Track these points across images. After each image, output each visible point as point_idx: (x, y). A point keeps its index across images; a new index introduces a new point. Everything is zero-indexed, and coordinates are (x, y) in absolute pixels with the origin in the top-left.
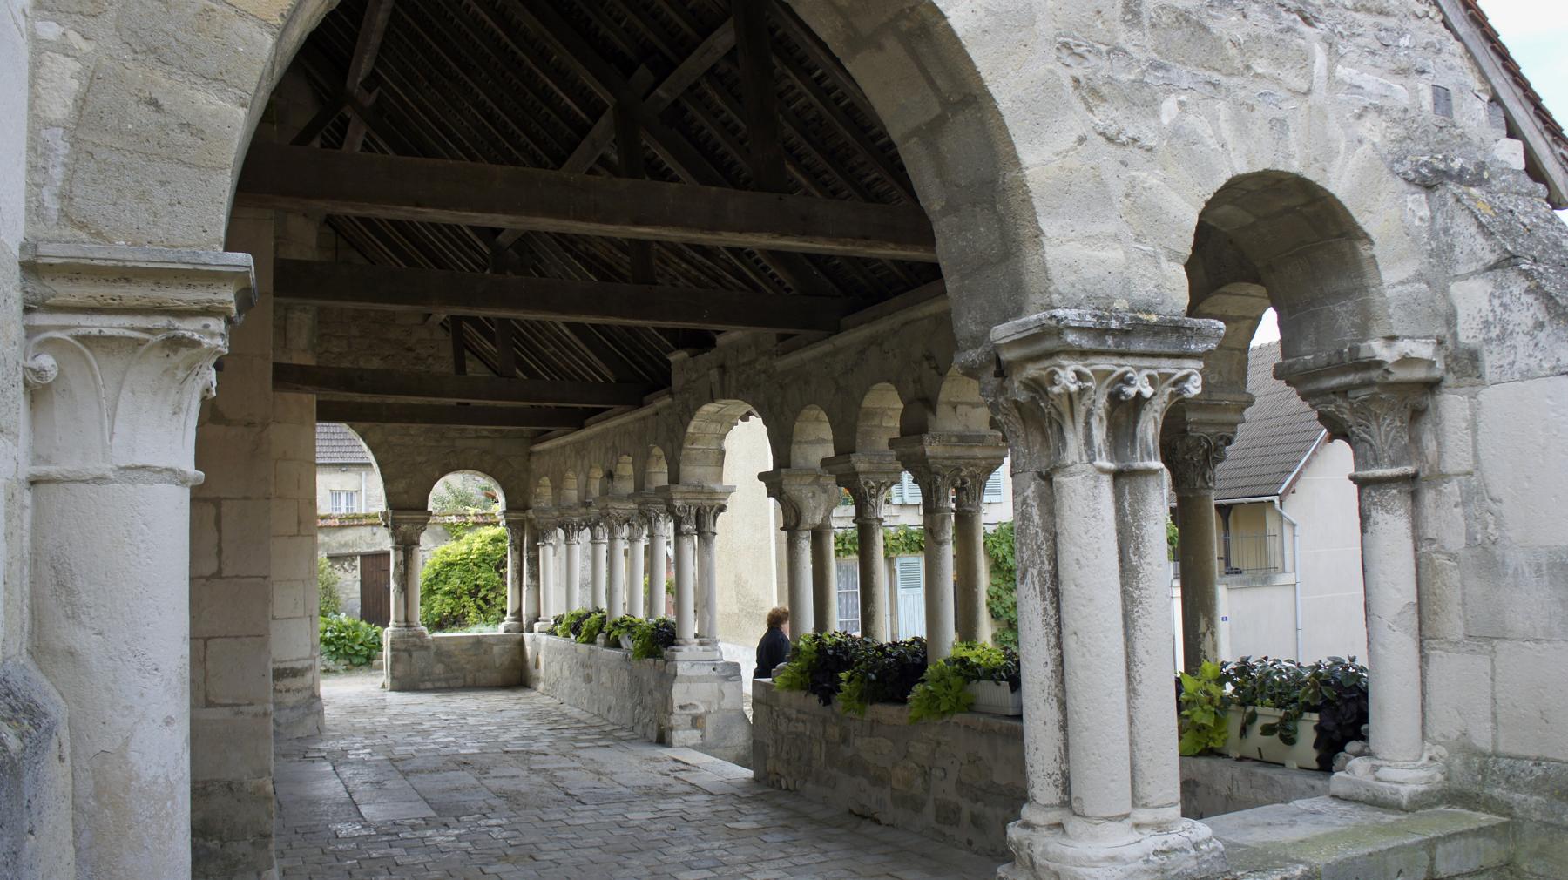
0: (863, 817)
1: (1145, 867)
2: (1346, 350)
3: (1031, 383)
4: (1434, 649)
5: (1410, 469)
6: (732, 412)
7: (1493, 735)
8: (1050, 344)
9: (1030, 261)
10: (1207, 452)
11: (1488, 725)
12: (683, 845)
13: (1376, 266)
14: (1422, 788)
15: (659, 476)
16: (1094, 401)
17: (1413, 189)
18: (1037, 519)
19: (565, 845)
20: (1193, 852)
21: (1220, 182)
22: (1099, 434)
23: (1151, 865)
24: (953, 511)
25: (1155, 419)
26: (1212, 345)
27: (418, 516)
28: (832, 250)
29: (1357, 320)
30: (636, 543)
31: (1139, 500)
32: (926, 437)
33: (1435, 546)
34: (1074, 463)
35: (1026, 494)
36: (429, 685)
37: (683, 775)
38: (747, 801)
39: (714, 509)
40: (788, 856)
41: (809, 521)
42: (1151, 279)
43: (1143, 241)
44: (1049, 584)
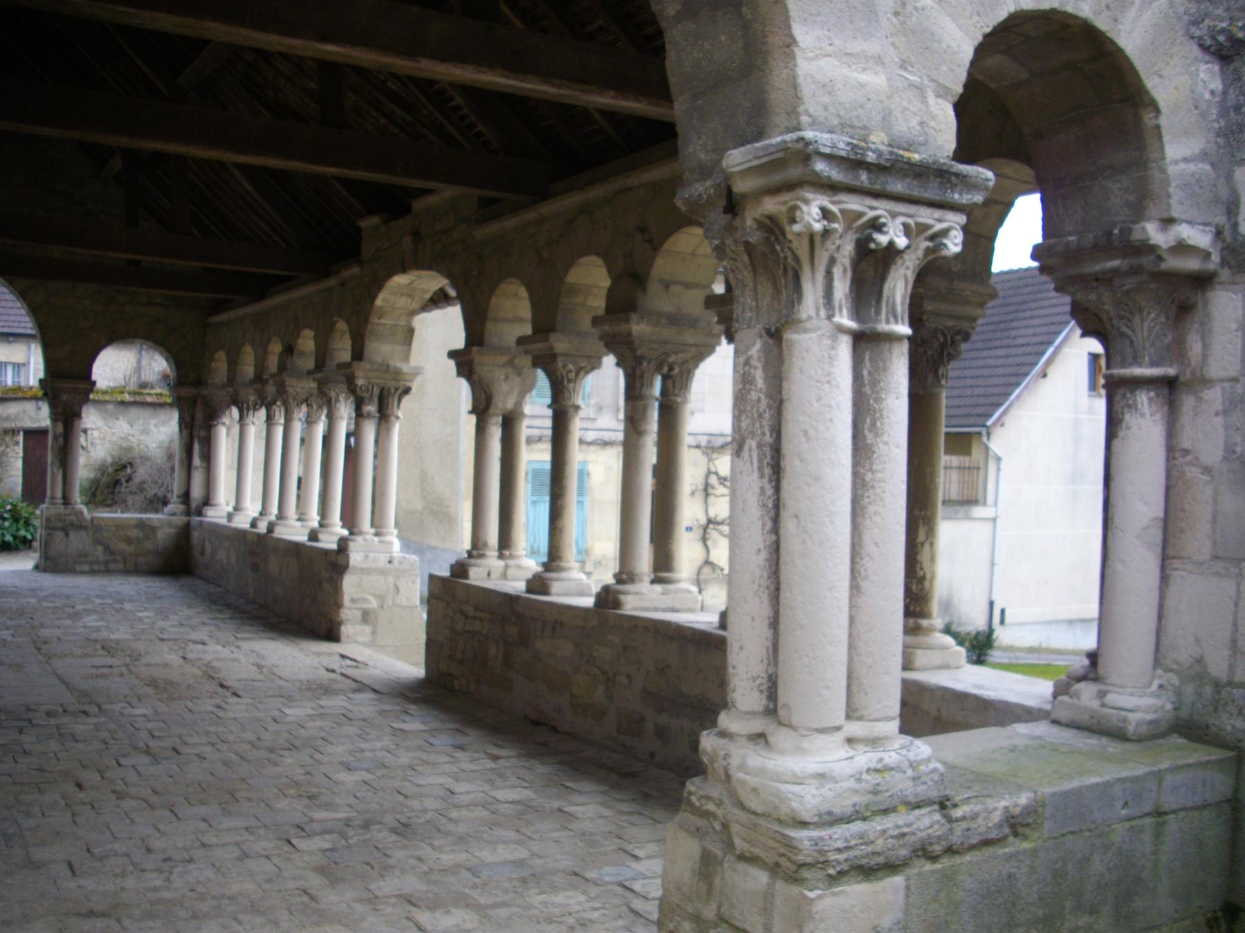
0: (537, 723)
1: (857, 786)
2: (1116, 231)
3: (768, 222)
4: (1177, 569)
5: (1171, 371)
6: (424, 286)
7: (1230, 665)
8: (794, 172)
9: (778, 77)
10: (943, 346)
11: (1226, 653)
12: (343, 744)
13: (1160, 137)
14: (1150, 717)
15: (343, 352)
16: (839, 248)
17: (1207, 58)
18: (760, 383)
19: (214, 739)
20: (910, 773)
21: (1001, 15)
22: (841, 288)
23: (863, 785)
24: (657, 399)
25: (906, 277)
26: (979, 198)
27: (81, 386)
28: (545, 93)
29: (1132, 198)
30: (314, 425)
31: (880, 368)
32: (634, 317)
33: (1189, 458)
34: (810, 318)
35: (749, 353)
36: (86, 568)
37: (350, 672)
38: (416, 701)
39: (400, 391)
40: (455, 761)
41: (500, 405)
42: (915, 114)
43: (910, 69)
44: (769, 457)
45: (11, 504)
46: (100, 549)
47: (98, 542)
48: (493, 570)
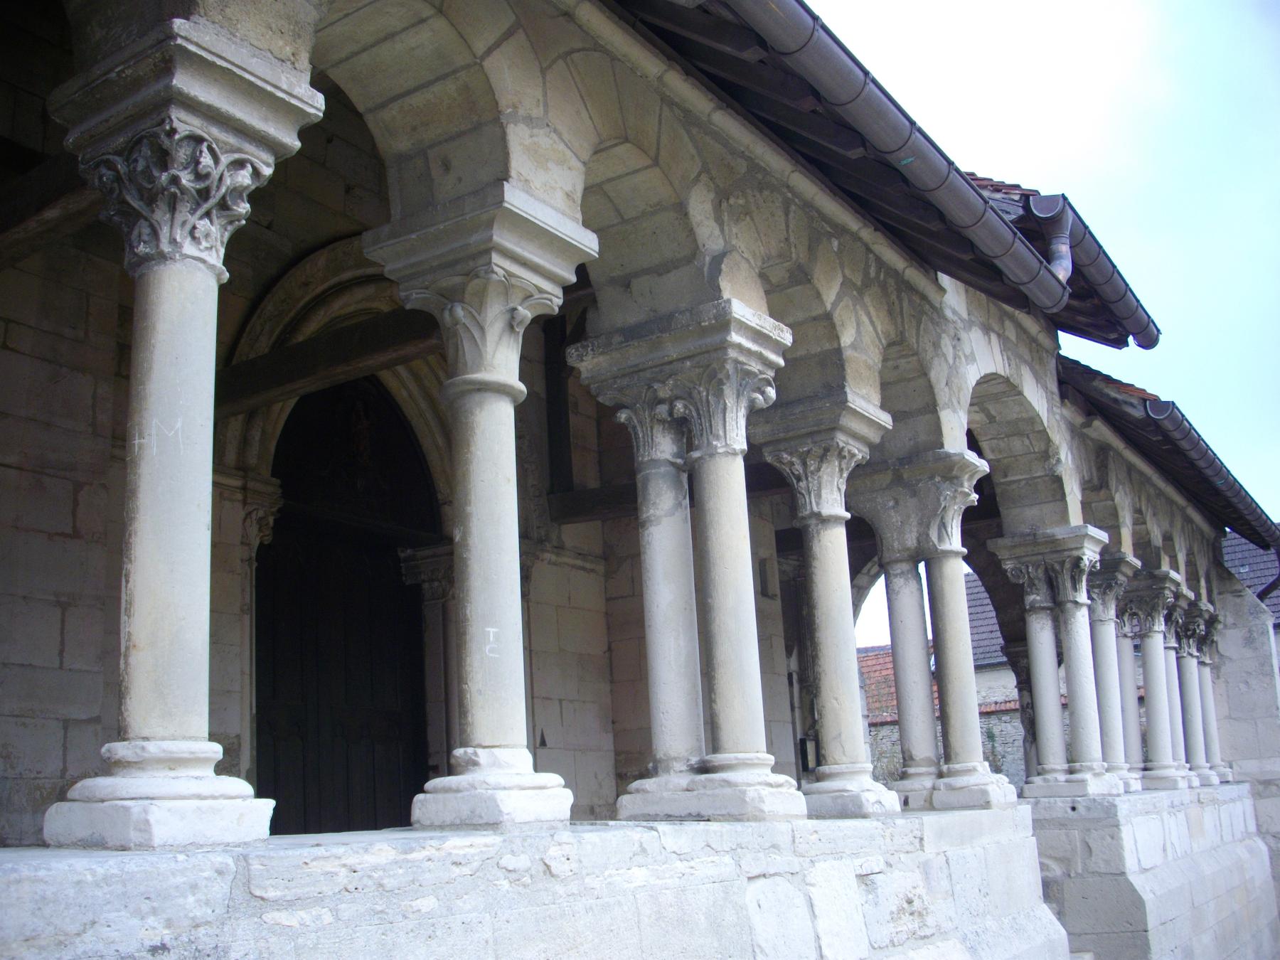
30: (1146, 639)
41: (896, 544)
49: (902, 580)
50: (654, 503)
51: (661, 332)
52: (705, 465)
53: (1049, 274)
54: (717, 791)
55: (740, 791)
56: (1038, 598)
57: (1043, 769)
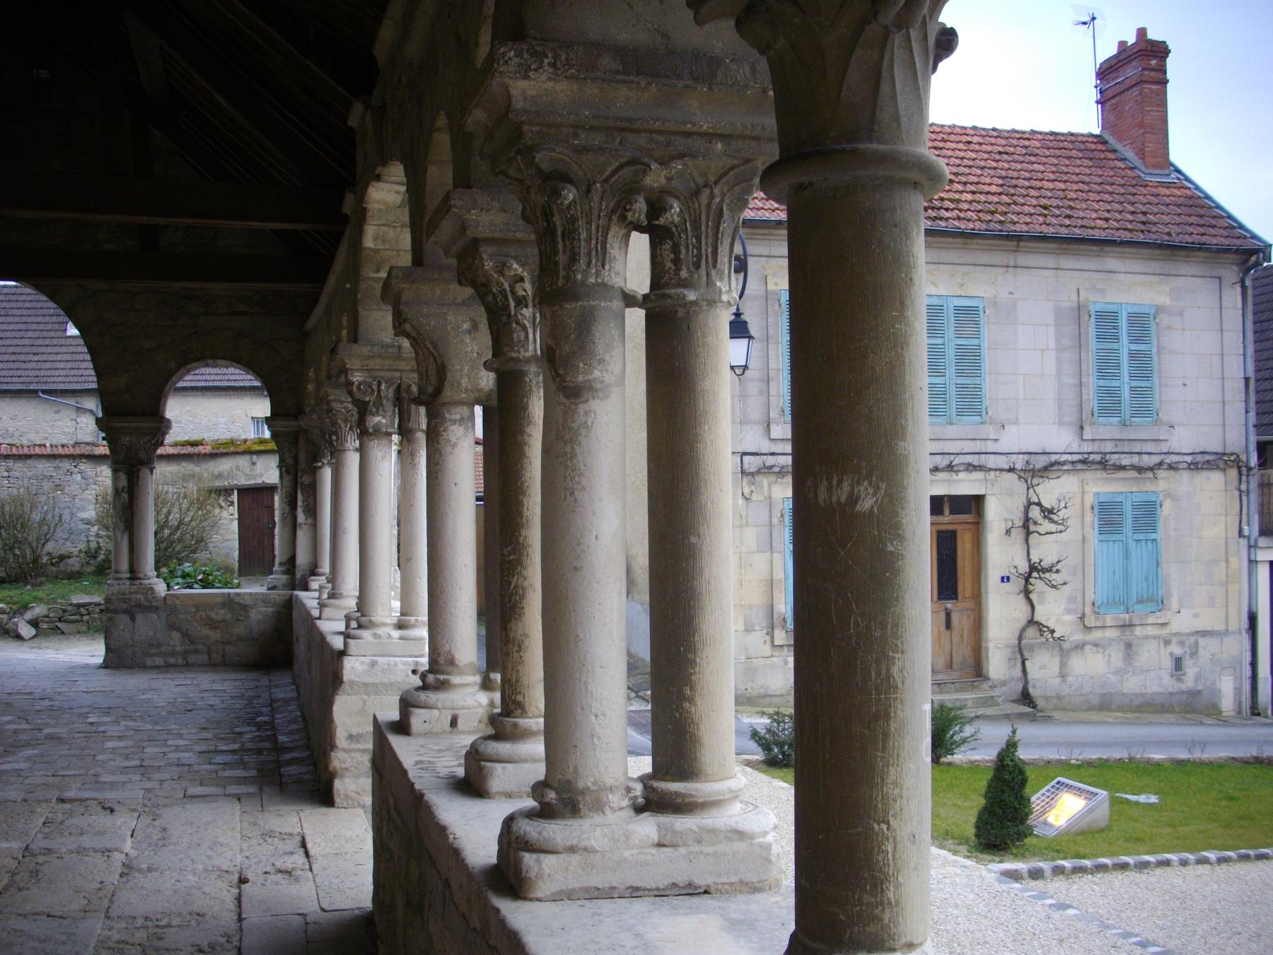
36: (159, 661)
41: (464, 382)
45: (204, 573)
46: (176, 636)
47: (172, 627)
48: (461, 713)
49: (461, 429)
50: (601, 361)
51: (696, 80)
52: (701, 317)
53: (1230, 614)
54: (722, 847)
55: (761, 845)
56: (384, 421)
57: (370, 621)
